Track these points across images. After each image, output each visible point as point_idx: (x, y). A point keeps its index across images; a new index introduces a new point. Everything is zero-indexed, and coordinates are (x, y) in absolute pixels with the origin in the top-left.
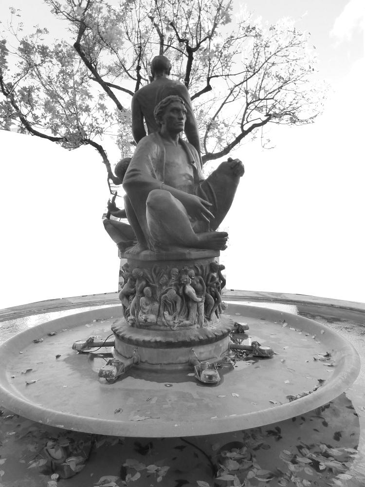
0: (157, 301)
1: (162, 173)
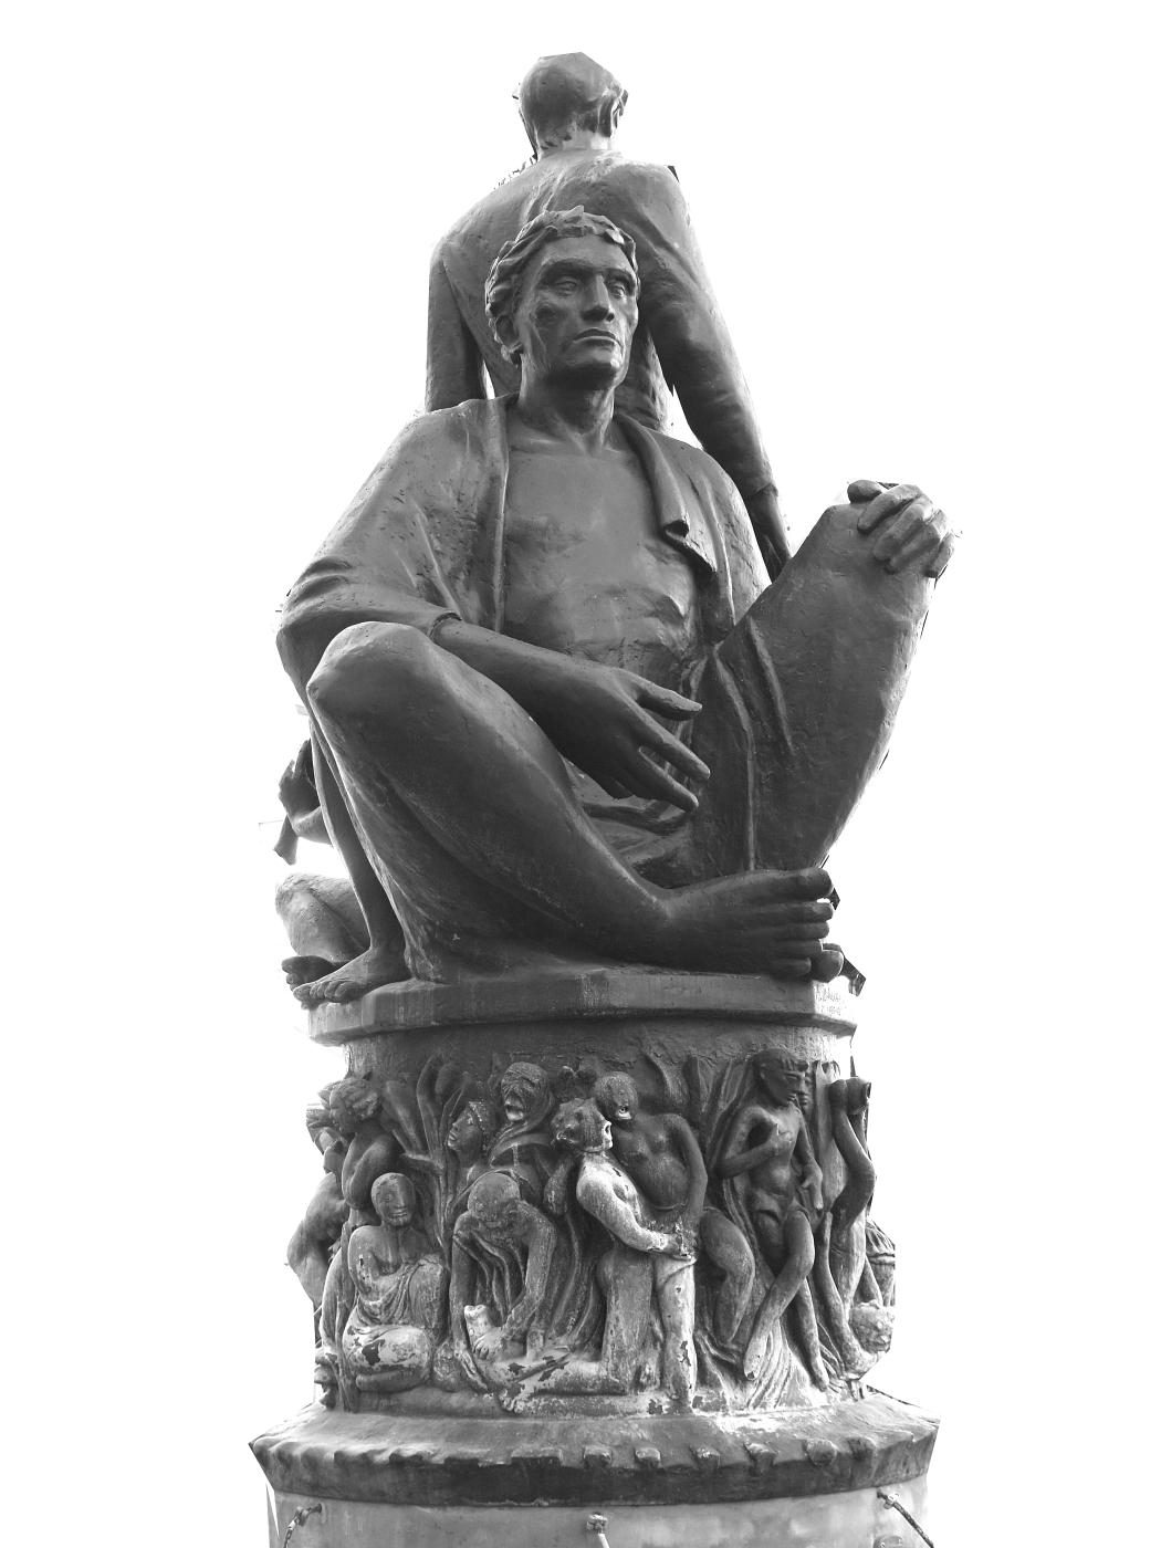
0: (435, 1249)
1: (488, 581)
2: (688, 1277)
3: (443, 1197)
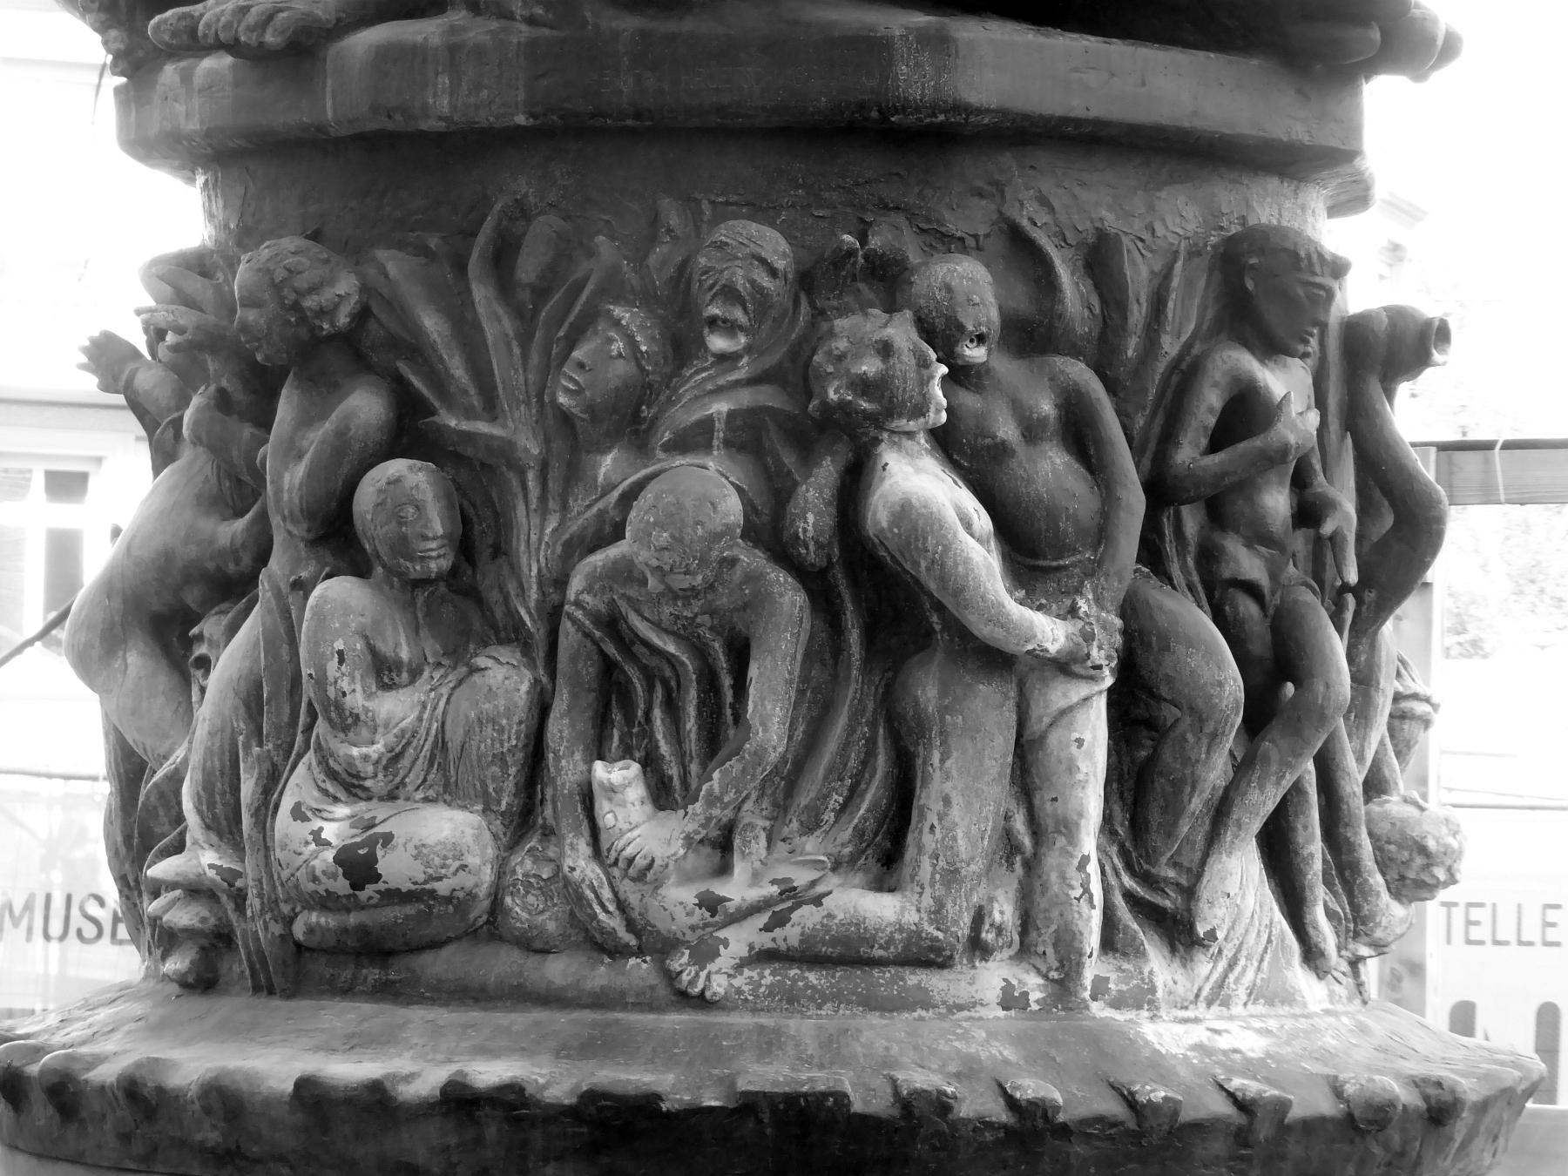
0: (513, 634)
2: (1098, 717)
3: (535, 520)
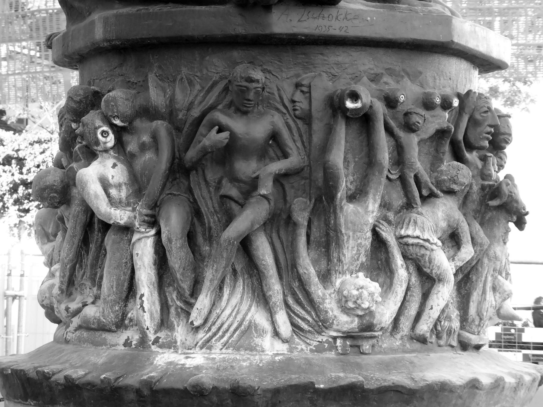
0: (146, 230)
